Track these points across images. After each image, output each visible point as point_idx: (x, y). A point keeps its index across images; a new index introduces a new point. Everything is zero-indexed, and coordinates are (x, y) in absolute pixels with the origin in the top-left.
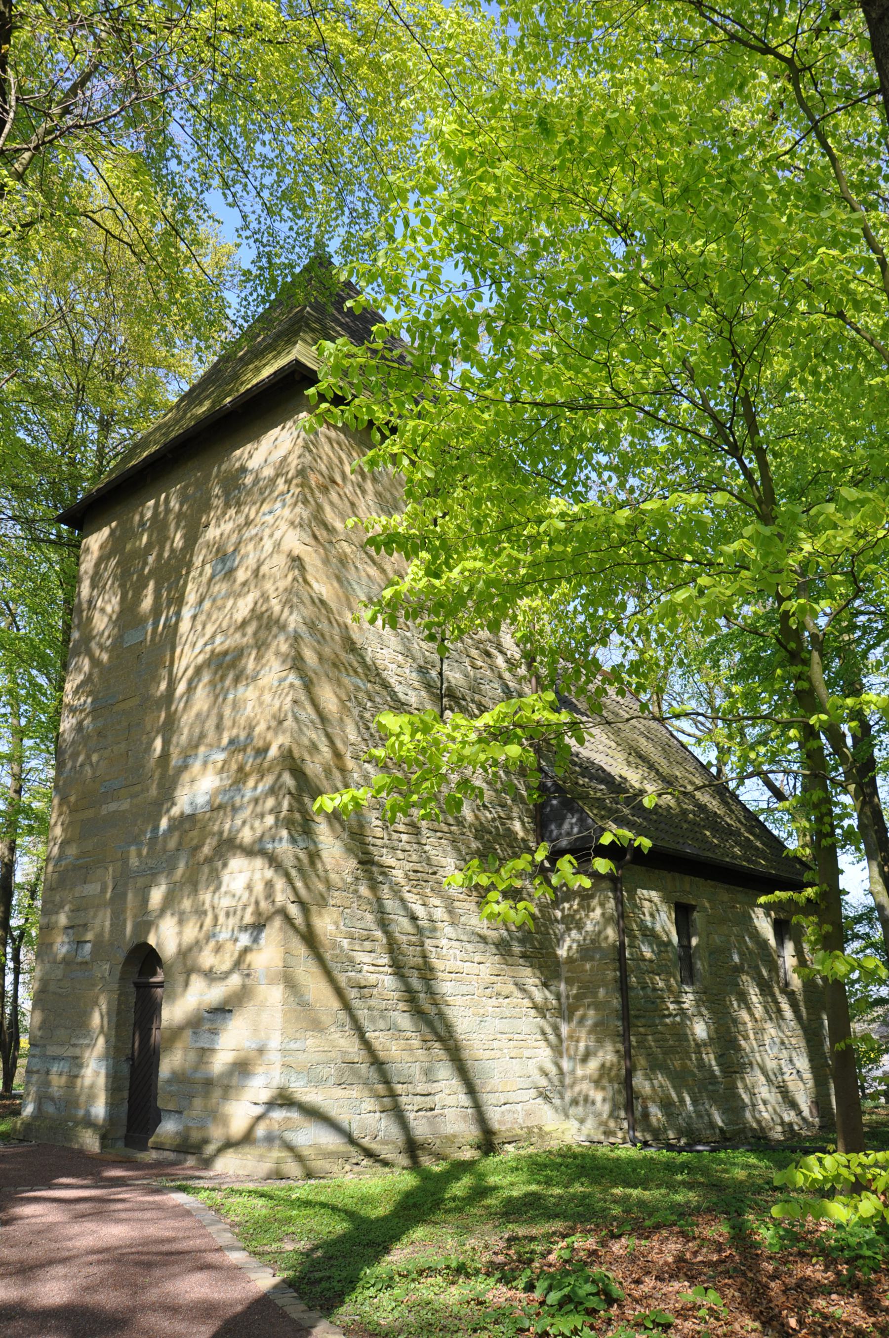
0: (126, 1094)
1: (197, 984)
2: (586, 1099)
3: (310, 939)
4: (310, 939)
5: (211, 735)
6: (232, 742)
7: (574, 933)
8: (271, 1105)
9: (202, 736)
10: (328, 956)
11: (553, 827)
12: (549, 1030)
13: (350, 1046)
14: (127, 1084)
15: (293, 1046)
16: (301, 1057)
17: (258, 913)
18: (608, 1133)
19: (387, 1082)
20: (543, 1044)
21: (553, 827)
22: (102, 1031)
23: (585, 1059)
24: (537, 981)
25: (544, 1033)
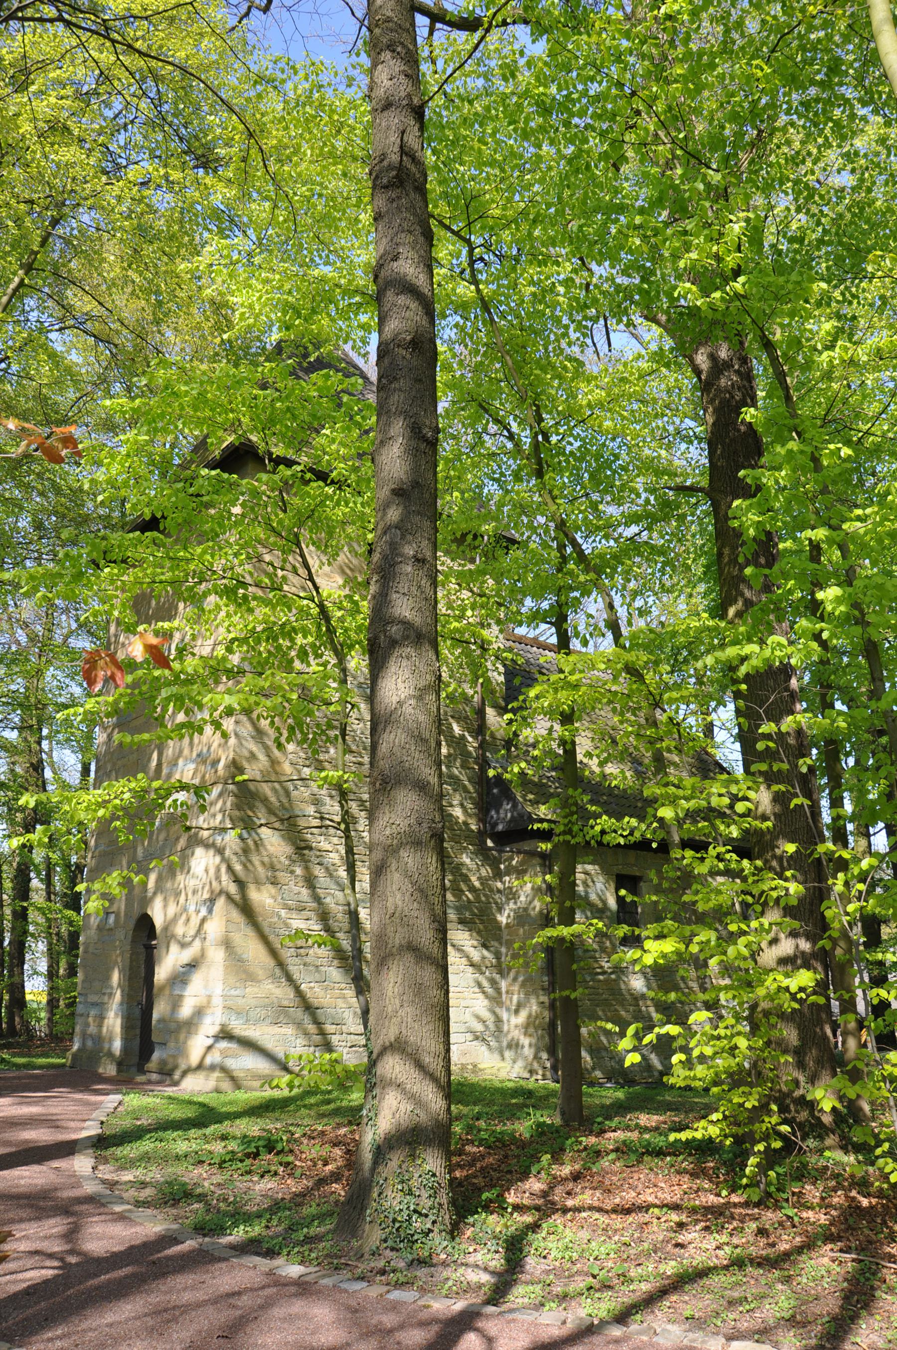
0: (138, 1031)
1: (174, 948)
2: (517, 1045)
3: (247, 910)
4: (247, 910)
5: (186, 752)
6: (199, 755)
7: (512, 905)
8: (217, 1038)
9: (181, 752)
10: (265, 925)
11: (493, 813)
12: (485, 984)
13: (283, 993)
14: (139, 1023)
15: (233, 992)
16: (241, 1001)
17: (212, 892)
18: (532, 1072)
19: (317, 1022)
20: (481, 996)
21: (493, 813)
22: (119, 985)
23: (517, 1012)
24: (475, 943)
25: (479, 985)
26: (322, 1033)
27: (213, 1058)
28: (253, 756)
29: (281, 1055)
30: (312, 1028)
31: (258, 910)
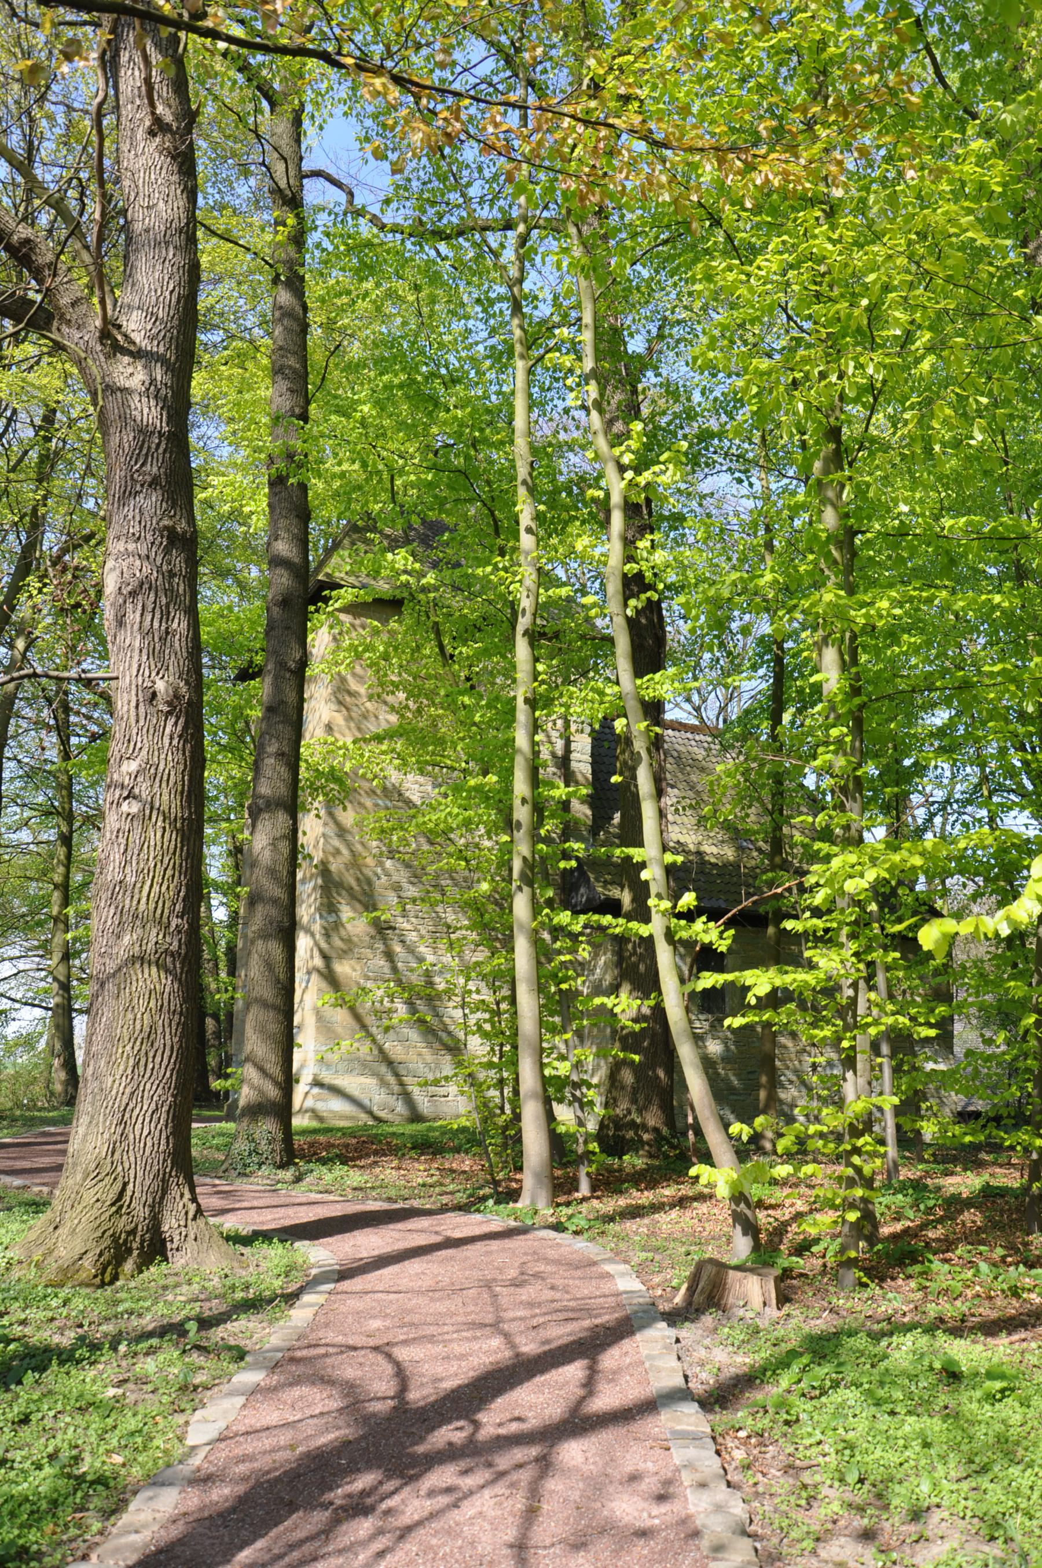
13: (365, 1049)
26: (402, 1084)
27: (309, 1103)
28: (337, 852)
29: (367, 1102)
30: (391, 1079)
31: (342, 979)
